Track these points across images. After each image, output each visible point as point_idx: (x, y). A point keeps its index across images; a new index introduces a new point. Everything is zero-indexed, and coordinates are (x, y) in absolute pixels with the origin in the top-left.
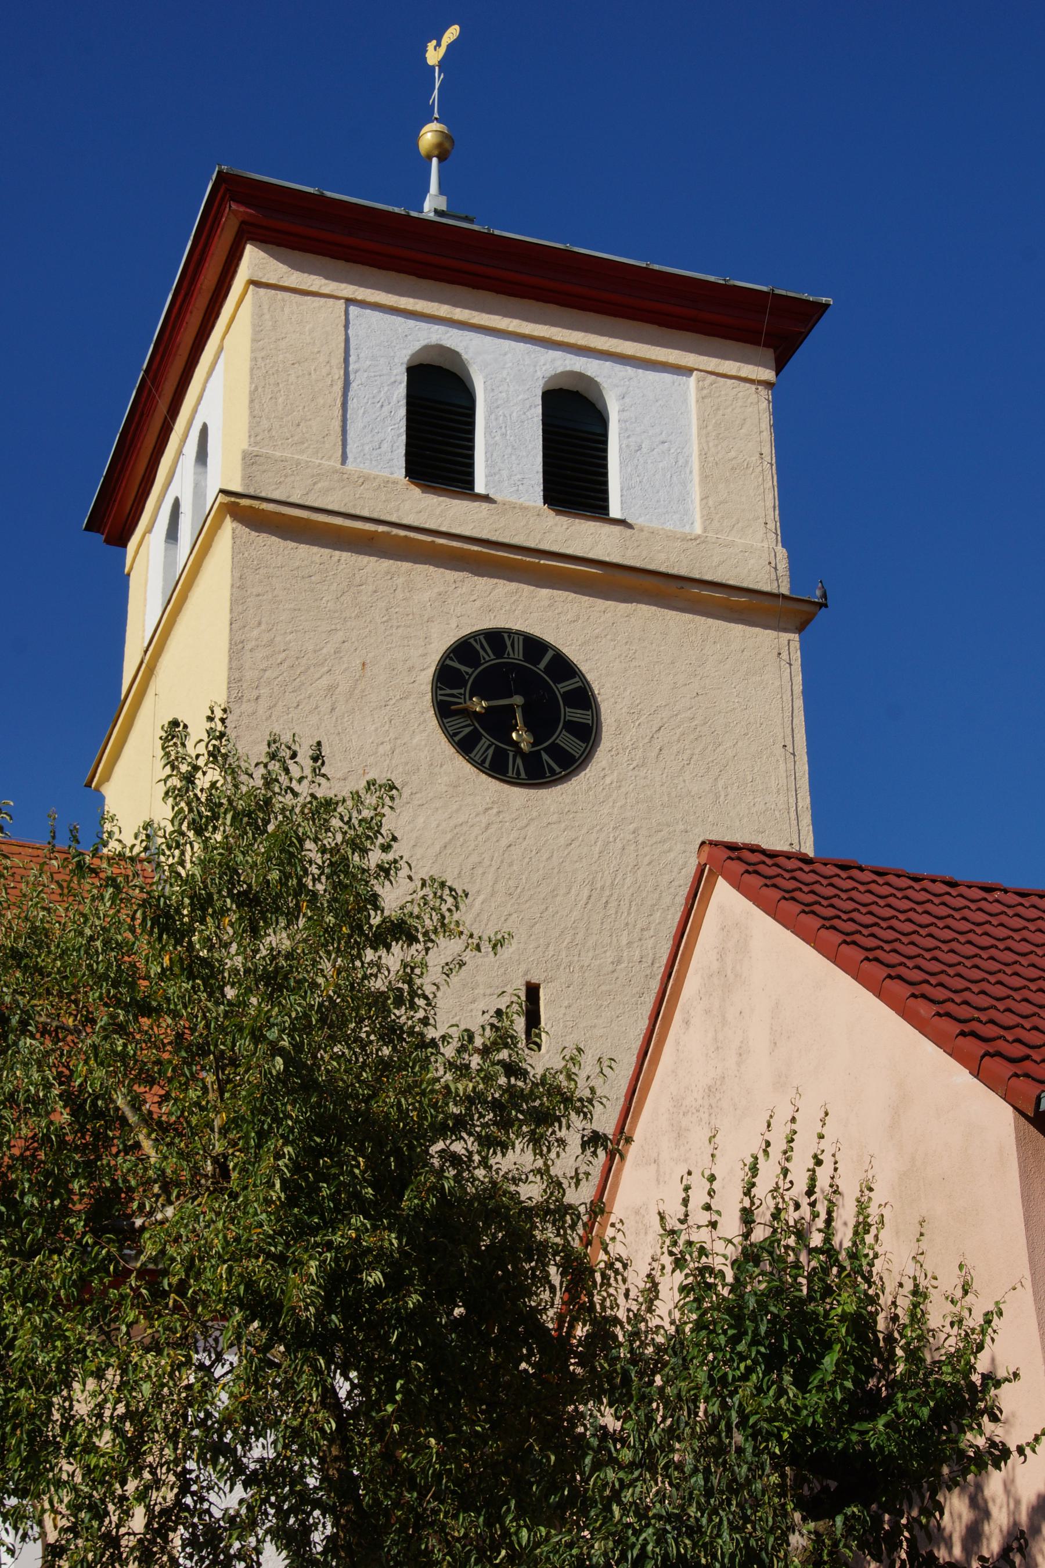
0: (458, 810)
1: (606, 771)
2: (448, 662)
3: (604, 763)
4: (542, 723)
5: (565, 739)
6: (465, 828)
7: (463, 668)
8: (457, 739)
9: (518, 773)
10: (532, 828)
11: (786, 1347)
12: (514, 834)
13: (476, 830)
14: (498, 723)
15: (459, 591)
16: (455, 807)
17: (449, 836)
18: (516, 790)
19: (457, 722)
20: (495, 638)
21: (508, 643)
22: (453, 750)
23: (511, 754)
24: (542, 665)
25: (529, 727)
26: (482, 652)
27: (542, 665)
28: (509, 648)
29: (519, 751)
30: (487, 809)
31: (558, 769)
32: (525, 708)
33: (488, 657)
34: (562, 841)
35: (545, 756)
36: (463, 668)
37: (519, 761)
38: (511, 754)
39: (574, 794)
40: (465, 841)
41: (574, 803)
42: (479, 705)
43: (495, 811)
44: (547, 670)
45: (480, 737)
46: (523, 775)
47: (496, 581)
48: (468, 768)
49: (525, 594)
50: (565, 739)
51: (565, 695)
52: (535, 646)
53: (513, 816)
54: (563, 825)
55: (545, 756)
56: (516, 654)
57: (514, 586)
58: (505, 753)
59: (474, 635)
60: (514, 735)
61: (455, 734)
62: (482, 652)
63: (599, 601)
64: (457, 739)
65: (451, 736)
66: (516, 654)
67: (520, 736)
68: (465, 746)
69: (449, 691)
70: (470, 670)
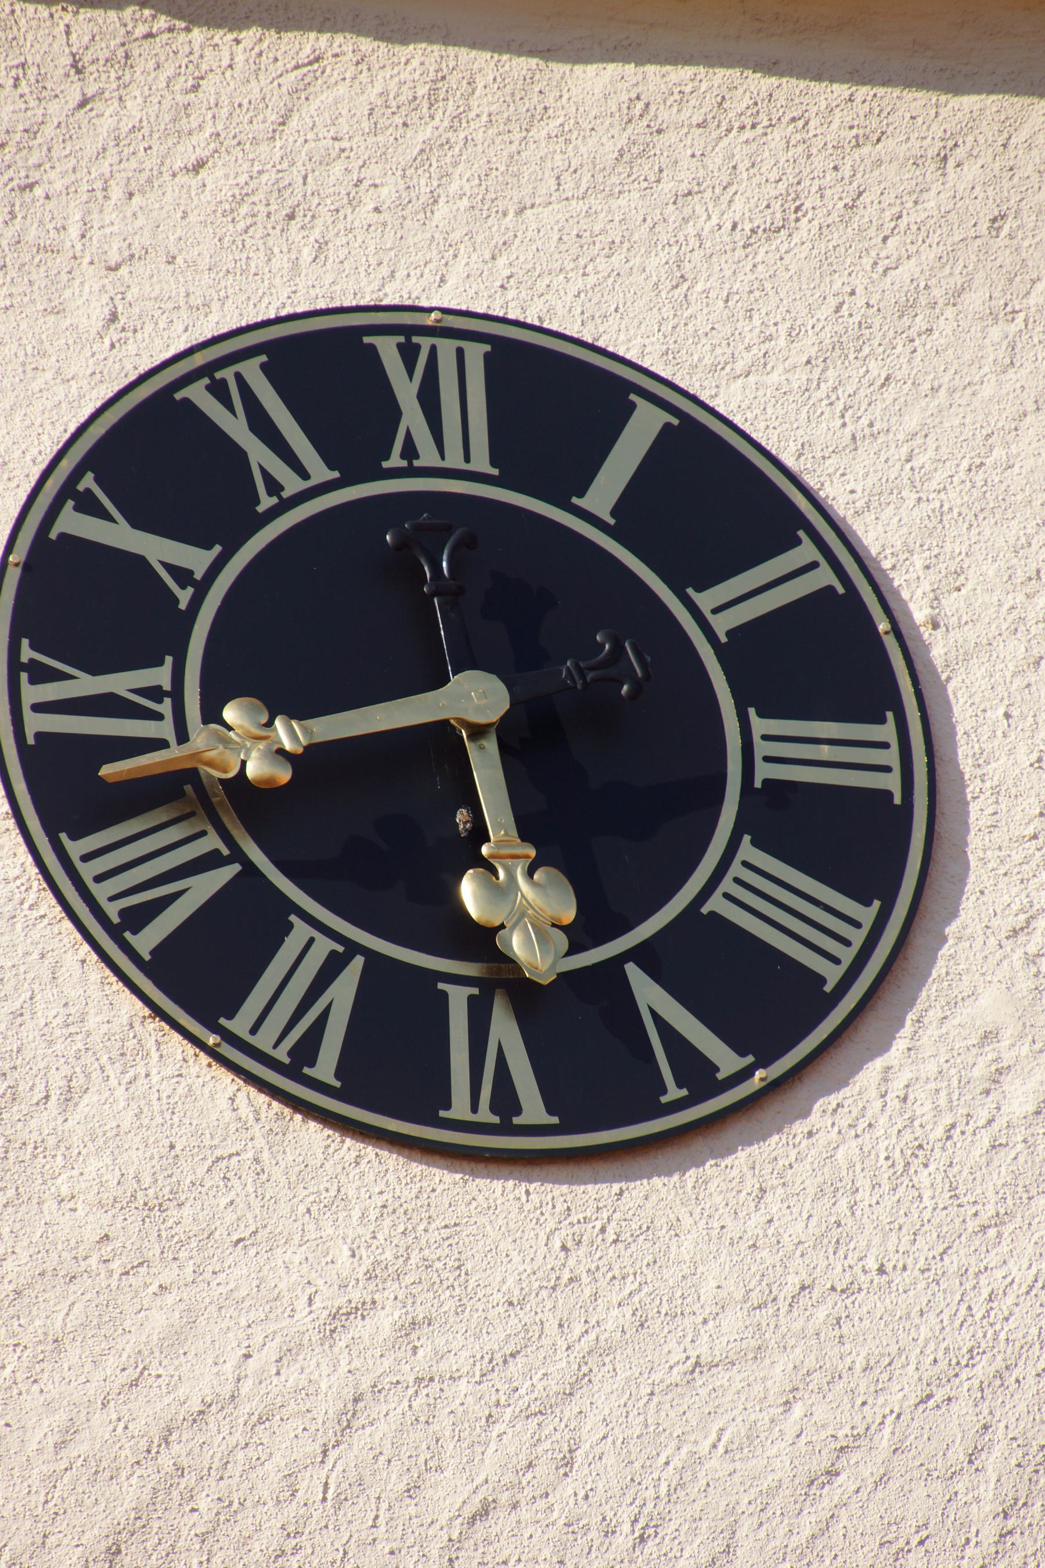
0: (174, 1341)
1: (1005, 1050)
2: (71, 522)
3: (989, 1006)
4: (615, 792)
5: (755, 892)
6: (220, 1436)
7: (158, 550)
8: (147, 940)
9: (506, 1100)
10: (603, 1398)
11: (579, 687)
12: (511, 1442)
13: (288, 1444)
14: (374, 834)
15: (106, 119)
16: (159, 1321)
17: (130, 1493)
18: (500, 1195)
19: (135, 852)
20: (331, 369)
21: (406, 390)
22: (130, 1005)
23: (458, 998)
24: (604, 493)
25: (550, 836)
26: (259, 455)
27: (604, 493)
28: (412, 418)
29: (504, 980)
30: (340, 1318)
31: (726, 1060)
32: (522, 738)
33: (296, 479)
34: (780, 1460)
35: (648, 994)
36: (158, 550)
37: (505, 1030)
38: (458, 998)
39: (829, 1190)
40: (228, 1509)
41: (835, 1238)
42: (253, 744)
43: (385, 1321)
44: (631, 518)
45: (277, 916)
46: (533, 1109)
47: (311, 42)
48: (218, 1099)
49: (482, 103)
50: (755, 892)
51: (741, 649)
52: (554, 394)
53: (494, 1342)
54: (778, 1372)
55: (648, 994)
56: (450, 448)
57: (418, 60)
58: (426, 988)
59: (212, 362)
60: (470, 892)
61: (138, 917)
62: (259, 455)
63: (913, 102)
64: (147, 940)
65: (110, 931)
66: (449, 446)
67: (520, 903)
68: (198, 977)
69: (86, 685)
70: (197, 559)
